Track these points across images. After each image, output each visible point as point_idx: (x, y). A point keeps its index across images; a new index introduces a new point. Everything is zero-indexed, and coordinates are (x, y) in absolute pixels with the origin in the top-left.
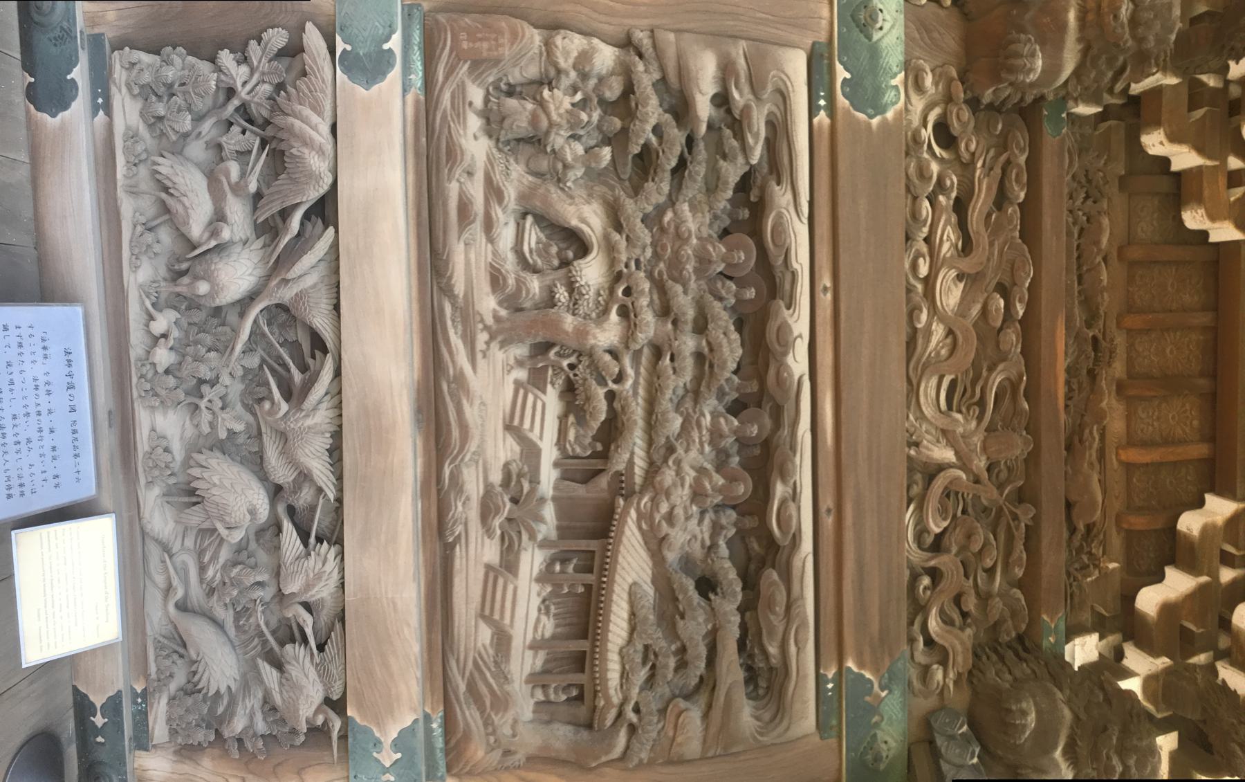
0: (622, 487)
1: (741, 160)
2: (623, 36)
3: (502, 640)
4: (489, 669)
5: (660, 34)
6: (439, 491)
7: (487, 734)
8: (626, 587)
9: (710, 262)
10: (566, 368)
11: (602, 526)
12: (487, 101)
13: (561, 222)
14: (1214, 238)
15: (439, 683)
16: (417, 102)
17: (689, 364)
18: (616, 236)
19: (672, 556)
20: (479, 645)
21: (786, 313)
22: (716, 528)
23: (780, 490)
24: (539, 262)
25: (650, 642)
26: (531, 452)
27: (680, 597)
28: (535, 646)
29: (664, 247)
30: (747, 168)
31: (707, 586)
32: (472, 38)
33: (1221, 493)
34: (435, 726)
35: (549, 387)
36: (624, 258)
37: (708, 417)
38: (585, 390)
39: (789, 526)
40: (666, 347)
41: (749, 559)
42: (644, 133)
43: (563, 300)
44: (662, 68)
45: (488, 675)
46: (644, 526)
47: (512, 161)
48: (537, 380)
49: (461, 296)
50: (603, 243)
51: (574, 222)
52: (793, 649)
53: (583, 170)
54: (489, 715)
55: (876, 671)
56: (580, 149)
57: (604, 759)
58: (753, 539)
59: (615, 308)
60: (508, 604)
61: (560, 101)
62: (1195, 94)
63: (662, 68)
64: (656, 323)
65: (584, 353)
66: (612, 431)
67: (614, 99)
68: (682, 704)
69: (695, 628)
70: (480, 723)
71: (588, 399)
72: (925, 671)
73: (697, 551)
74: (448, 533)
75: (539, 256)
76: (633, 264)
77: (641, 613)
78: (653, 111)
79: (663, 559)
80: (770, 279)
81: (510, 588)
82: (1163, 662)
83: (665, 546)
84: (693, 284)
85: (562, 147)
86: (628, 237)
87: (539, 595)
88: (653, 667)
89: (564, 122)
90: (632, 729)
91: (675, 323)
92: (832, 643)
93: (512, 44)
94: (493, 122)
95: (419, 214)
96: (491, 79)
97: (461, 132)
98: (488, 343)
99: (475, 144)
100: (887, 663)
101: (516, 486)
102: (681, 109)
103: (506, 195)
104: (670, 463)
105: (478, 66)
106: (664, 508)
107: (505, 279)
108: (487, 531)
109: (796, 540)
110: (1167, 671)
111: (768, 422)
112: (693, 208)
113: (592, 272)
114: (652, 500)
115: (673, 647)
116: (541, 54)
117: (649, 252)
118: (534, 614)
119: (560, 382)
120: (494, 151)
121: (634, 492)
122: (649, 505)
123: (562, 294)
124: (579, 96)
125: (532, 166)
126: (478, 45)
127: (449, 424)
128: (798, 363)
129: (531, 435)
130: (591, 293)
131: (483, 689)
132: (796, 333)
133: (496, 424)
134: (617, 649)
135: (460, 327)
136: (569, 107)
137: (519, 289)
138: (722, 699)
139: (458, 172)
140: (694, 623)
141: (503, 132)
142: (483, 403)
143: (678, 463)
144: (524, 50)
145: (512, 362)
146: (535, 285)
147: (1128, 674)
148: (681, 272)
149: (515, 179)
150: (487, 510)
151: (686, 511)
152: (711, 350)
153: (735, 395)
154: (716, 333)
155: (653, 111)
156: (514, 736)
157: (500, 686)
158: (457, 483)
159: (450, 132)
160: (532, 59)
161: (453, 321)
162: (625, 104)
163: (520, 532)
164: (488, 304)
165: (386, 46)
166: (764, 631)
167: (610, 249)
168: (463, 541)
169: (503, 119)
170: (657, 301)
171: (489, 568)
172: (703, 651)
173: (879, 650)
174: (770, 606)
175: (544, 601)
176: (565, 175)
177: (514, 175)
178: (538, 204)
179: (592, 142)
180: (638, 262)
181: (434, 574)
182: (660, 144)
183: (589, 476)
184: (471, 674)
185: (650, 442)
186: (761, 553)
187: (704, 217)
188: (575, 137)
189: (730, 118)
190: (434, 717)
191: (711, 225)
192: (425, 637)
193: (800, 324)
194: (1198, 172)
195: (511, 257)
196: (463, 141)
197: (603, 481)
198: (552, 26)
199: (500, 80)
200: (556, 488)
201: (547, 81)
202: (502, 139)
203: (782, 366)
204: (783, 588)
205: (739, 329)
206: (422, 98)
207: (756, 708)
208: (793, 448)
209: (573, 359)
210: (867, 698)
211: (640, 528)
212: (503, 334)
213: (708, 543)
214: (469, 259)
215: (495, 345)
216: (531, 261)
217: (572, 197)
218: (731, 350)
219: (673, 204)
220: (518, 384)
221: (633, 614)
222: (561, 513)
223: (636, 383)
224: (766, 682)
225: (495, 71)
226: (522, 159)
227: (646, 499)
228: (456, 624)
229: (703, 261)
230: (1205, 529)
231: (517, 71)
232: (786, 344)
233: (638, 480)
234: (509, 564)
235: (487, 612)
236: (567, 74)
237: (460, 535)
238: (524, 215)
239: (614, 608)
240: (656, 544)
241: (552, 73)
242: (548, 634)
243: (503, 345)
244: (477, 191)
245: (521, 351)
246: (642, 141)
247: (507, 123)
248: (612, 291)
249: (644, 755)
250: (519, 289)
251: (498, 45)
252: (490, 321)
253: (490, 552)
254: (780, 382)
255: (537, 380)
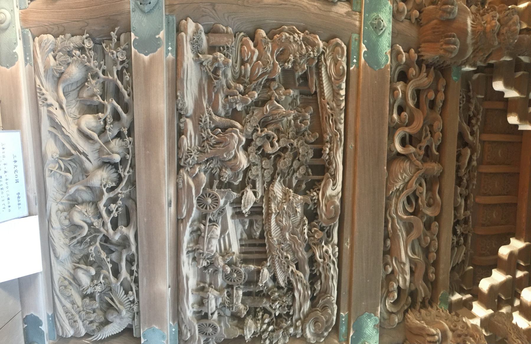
14: (506, 96)
33: (518, 238)
62: (518, 65)
82: (490, 311)
110: (491, 316)
147: (473, 316)
165: (157, 37)
194: (514, 99)
230: (511, 254)
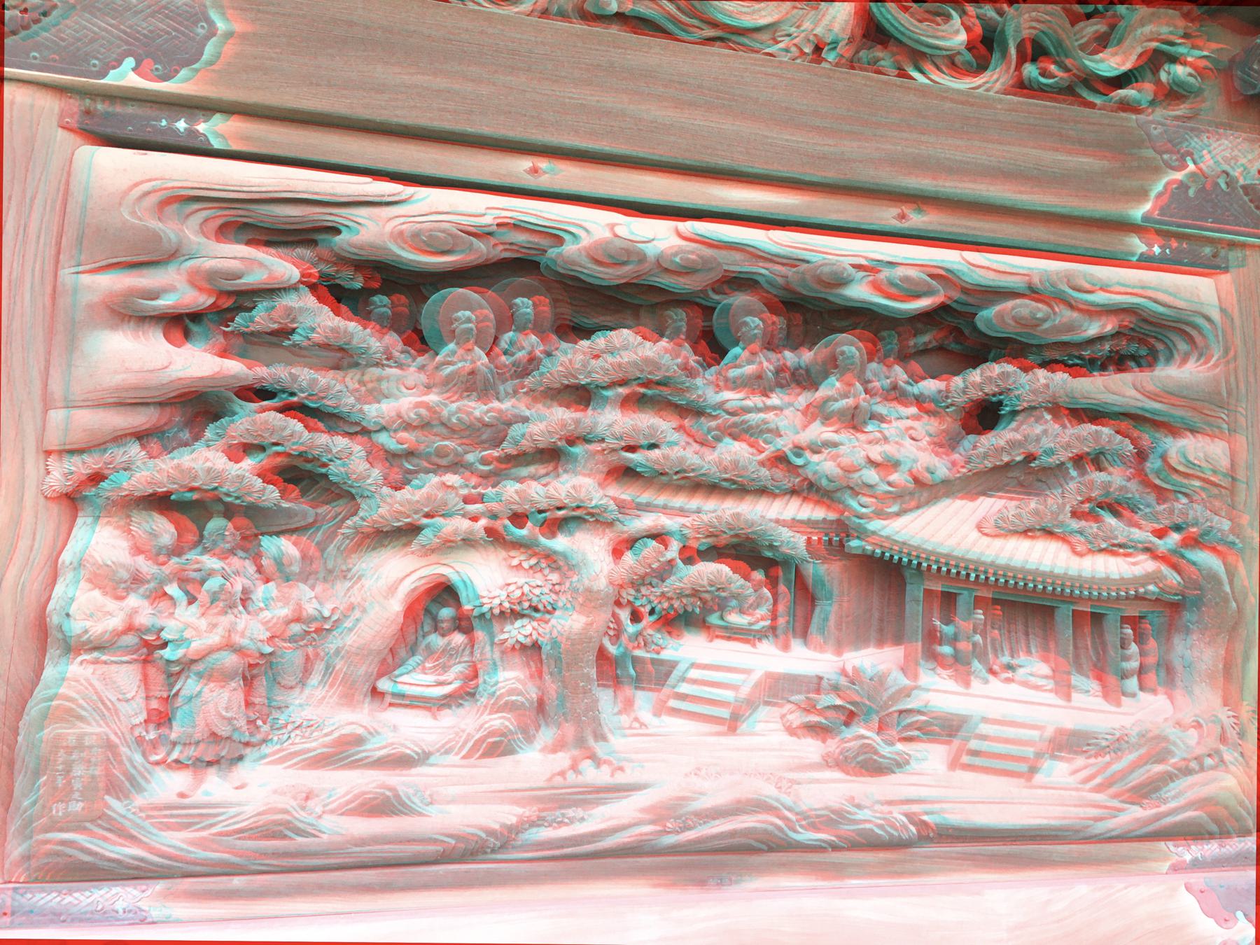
0: (836, 540)
1: (290, 300)
2: (55, 509)
3: (1068, 743)
4: (1109, 764)
5: (54, 440)
6: (835, 848)
7: (1202, 769)
8: (986, 540)
9: (472, 373)
10: (639, 626)
11: (888, 573)
12: (179, 764)
13: (395, 628)
15: (1124, 848)
16: (168, 895)
17: (646, 421)
18: (426, 537)
19: (941, 468)
20: (1072, 781)
21: (570, 248)
22: (896, 394)
23: (860, 292)
24: (458, 668)
25: (1068, 508)
26: (776, 688)
27: (1006, 459)
28: (1065, 690)
29: (441, 453)
30: (304, 290)
31: (985, 415)
32: (65, 794)
34: (1188, 857)
35: (665, 655)
36: (465, 524)
37: (727, 395)
38: (680, 596)
39: (917, 283)
40: (613, 458)
41: (941, 349)
42: (244, 476)
43: (528, 630)
44: (119, 438)
45: (1117, 767)
46: (895, 508)
47: (283, 718)
48: (657, 675)
49: (519, 810)
50: (434, 558)
51: (396, 606)
52: (1100, 298)
53: (301, 585)
54: (1174, 766)
55: (1156, 171)
56: (262, 592)
57: (1227, 589)
58: (911, 343)
59: (543, 541)
60: (1011, 732)
61: (189, 626)
63: (119, 438)
64: (575, 473)
65: (623, 600)
66: (745, 551)
67: (172, 529)
68: (1153, 464)
69: (1053, 438)
70: (1190, 780)
71: (695, 593)
72: (1173, 94)
73: (927, 427)
74: (905, 836)
75: (445, 668)
76: (473, 508)
77: (1028, 521)
78: (204, 461)
79: (945, 482)
80: (513, 268)
81: (985, 729)
83: (927, 477)
84: (506, 405)
85: (265, 623)
86: (428, 516)
87: (986, 682)
88: (1100, 506)
89: (225, 620)
90: (1193, 542)
91: (571, 441)
92: (1097, 234)
93: (80, 718)
94: (220, 752)
95: (368, 889)
96: (138, 758)
97: (232, 811)
98: (598, 762)
99: (255, 788)
100: (1150, 153)
101: (835, 713)
102: (199, 407)
103: (347, 730)
104: (799, 462)
105: (120, 784)
106: (871, 476)
107: (492, 733)
108: (899, 765)
109: (943, 277)
111: (740, 299)
112: (376, 395)
113: (486, 578)
114: (855, 493)
115: (1074, 473)
116: (96, 662)
117: (452, 479)
118: (1014, 690)
119: (658, 637)
120: (266, 749)
121: (839, 521)
122: (864, 500)
123: (519, 631)
124: (173, 590)
125: (291, 681)
126: (77, 785)
127: (733, 834)
128: (659, 237)
129: (745, 691)
130: (521, 581)
131: (1137, 777)
132: (607, 234)
133: (727, 748)
134: (1076, 559)
135: (570, 812)
136: (194, 608)
137: (510, 707)
138: (1157, 406)
139: (303, 818)
140: (1044, 440)
141: (236, 736)
142: (697, 771)
143: (799, 450)
144: (93, 695)
145: (625, 720)
146: (509, 678)
148: (486, 425)
149: (316, 710)
150: (872, 767)
151: (877, 442)
152: (623, 383)
153: (687, 350)
154: (599, 371)
155: (204, 461)
156: (1198, 726)
157: (1134, 747)
158: (832, 818)
159: (228, 834)
160: (104, 678)
161: (561, 824)
162: (187, 508)
163: (901, 712)
164: (535, 763)
166: (1065, 338)
167: (448, 545)
168: (915, 808)
169: (214, 734)
170: (532, 469)
171: (954, 764)
172: (1088, 428)
173: (1133, 161)
174: (1036, 323)
175: (992, 672)
176: (312, 619)
177: (309, 713)
178: (362, 671)
179: (251, 568)
180: (467, 500)
181: (964, 857)
182: (262, 448)
183: (806, 594)
184: (1115, 796)
185: (763, 492)
186: (953, 332)
187: (388, 378)
188: (245, 600)
189: (221, 312)
190: (1175, 859)
191: (400, 366)
192: (1061, 872)
193: (595, 226)
195: (449, 718)
196: (250, 810)
197: (815, 570)
198: (44, 636)
199: (140, 740)
200: (821, 649)
201: (148, 648)
202: (246, 738)
203: (661, 265)
204: (1010, 304)
205: (587, 333)
206: (160, 886)
207: (1170, 358)
208: (793, 262)
209: (624, 615)
210: (1191, 193)
211: (898, 514)
212: (585, 737)
213: (913, 410)
214: (459, 798)
215: (600, 749)
216: (456, 685)
217: (351, 608)
218: (626, 347)
219: (365, 432)
220: (661, 709)
221: (1026, 533)
222: (860, 641)
223: (665, 509)
224: (1142, 338)
225: (124, 750)
226: (280, 697)
227: (853, 504)
228: (1044, 822)
229: (474, 385)
231: (124, 708)
232: (628, 254)
233: (819, 513)
234: (946, 729)
235: (1023, 767)
236: (135, 611)
237: (906, 815)
238: (375, 693)
239: (1017, 562)
240: (925, 490)
241: (131, 640)
242: (1045, 669)
243: (601, 737)
244: (346, 783)
245: (605, 699)
246: (258, 482)
247: (224, 730)
248: (517, 545)
249: (1226, 525)
250: (510, 707)
251: (80, 746)
252: (562, 760)
253: (930, 759)
254: (687, 270)
255: (657, 675)
